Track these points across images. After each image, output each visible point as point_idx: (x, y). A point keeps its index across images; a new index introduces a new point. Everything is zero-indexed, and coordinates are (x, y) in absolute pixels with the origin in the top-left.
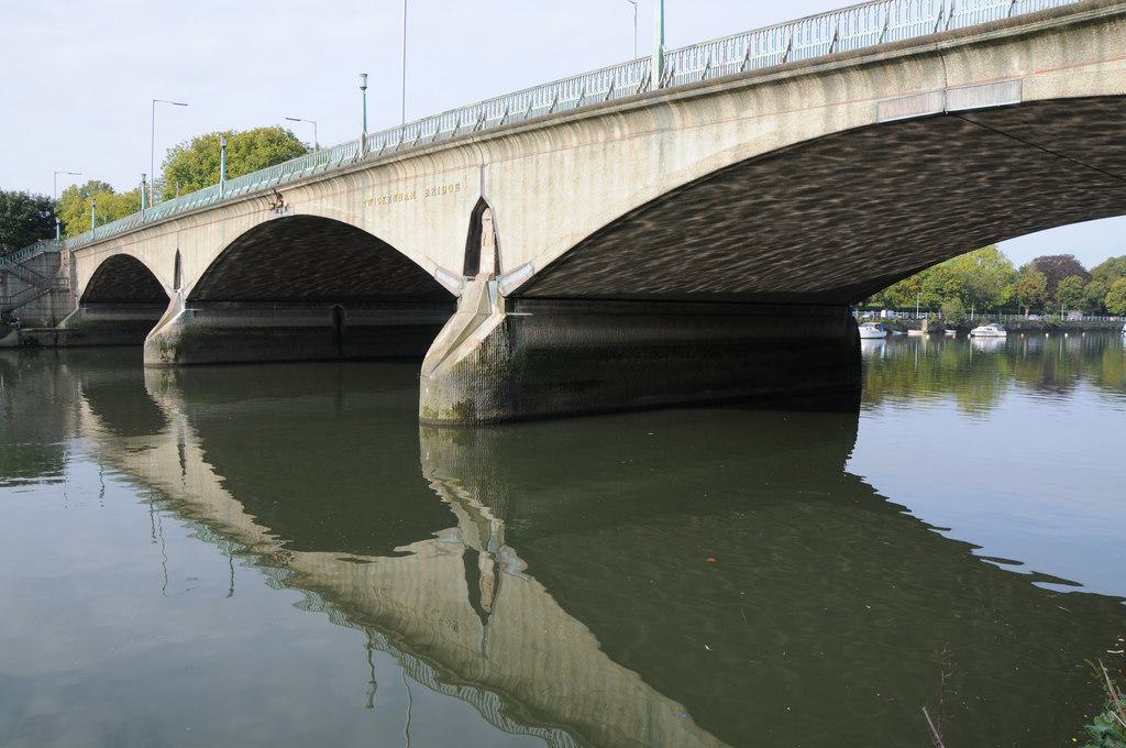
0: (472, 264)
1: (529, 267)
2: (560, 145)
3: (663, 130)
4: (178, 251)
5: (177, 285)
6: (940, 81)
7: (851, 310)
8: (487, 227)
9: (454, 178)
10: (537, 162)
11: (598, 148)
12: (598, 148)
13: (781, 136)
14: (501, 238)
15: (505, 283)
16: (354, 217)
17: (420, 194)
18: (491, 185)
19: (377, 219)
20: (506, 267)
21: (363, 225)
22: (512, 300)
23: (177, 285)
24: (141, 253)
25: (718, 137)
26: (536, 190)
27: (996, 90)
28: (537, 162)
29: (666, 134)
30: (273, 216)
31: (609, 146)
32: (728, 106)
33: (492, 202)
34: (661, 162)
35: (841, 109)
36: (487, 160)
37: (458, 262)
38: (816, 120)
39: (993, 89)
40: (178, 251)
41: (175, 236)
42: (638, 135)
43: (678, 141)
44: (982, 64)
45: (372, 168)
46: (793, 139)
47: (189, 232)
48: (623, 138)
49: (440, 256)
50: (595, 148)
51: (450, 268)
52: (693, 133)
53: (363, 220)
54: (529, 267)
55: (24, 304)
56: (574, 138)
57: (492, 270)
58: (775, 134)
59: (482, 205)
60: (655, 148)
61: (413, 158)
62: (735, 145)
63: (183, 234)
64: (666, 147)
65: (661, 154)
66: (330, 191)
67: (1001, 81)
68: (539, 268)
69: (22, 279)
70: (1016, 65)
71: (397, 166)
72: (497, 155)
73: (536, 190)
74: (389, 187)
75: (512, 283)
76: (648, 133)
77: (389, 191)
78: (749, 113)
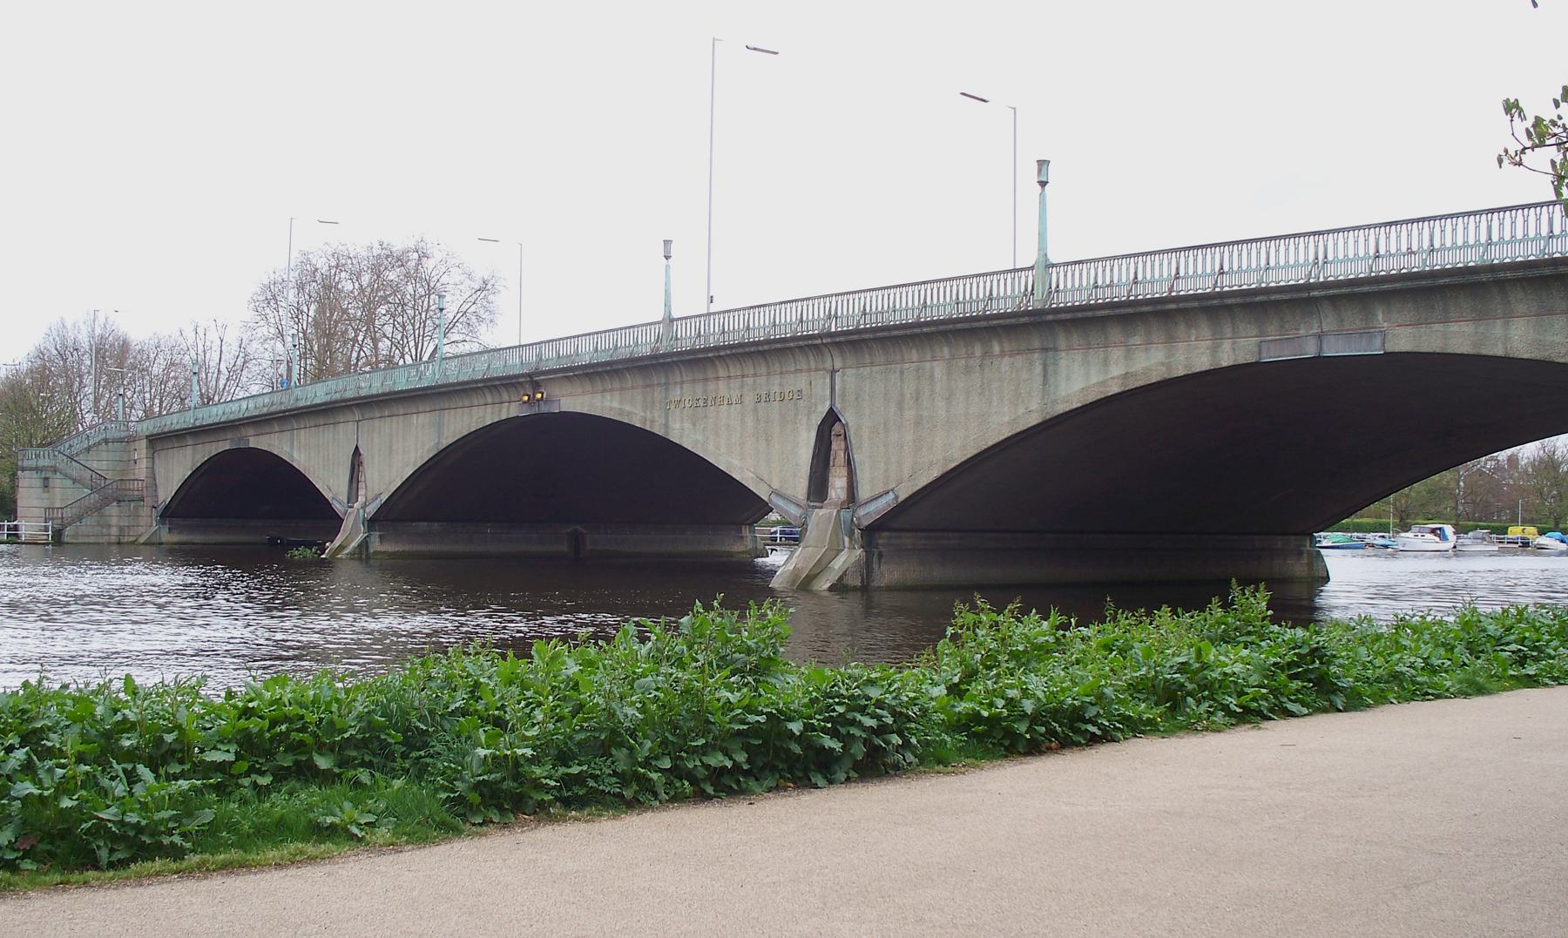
0: (818, 488)
1: (891, 495)
2: (929, 357)
3: (1047, 350)
4: (357, 451)
5: (353, 495)
6: (1316, 325)
7: (122, 747)
8: (837, 446)
9: (801, 381)
10: (902, 372)
11: (974, 363)
12: (974, 363)
13: (1169, 367)
14: (857, 457)
15: (862, 512)
16: (652, 422)
17: (749, 399)
18: (843, 395)
19: (687, 425)
20: (864, 492)
21: (667, 434)
22: (871, 533)
23: (353, 495)
24: (711, 447)
25: (1106, 362)
26: (900, 406)
27: (1364, 340)
28: (902, 372)
29: (1050, 354)
30: (525, 412)
31: (987, 362)
32: (1115, 334)
33: (847, 417)
34: (1044, 385)
35: (1227, 345)
36: (838, 364)
37: (344, 497)
38: (1203, 353)
39: (1361, 337)
40: (357, 451)
41: (351, 427)
42: (1019, 352)
43: (1063, 363)
44: (1353, 319)
45: (681, 361)
46: (1180, 371)
47: (377, 422)
48: (1002, 354)
49: (331, 482)
50: (971, 362)
51: (789, 492)
52: (1078, 356)
53: (666, 426)
54: (891, 495)
55: (80, 519)
56: (946, 350)
57: (843, 495)
58: (1162, 364)
59: (832, 418)
60: (1038, 369)
61: (741, 354)
62: (1123, 373)
63: (365, 425)
64: (1051, 368)
65: (1044, 376)
66: (617, 384)
67: (1366, 333)
68: (903, 496)
69: (75, 481)
70: (1380, 318)
71: (728, 361)
72: (850, 360)
73: (900, 406)
74: (682, 388)
75: (870, 512)
76: (1031, 351)
77: (705, 392)
78: (1137, 340)
